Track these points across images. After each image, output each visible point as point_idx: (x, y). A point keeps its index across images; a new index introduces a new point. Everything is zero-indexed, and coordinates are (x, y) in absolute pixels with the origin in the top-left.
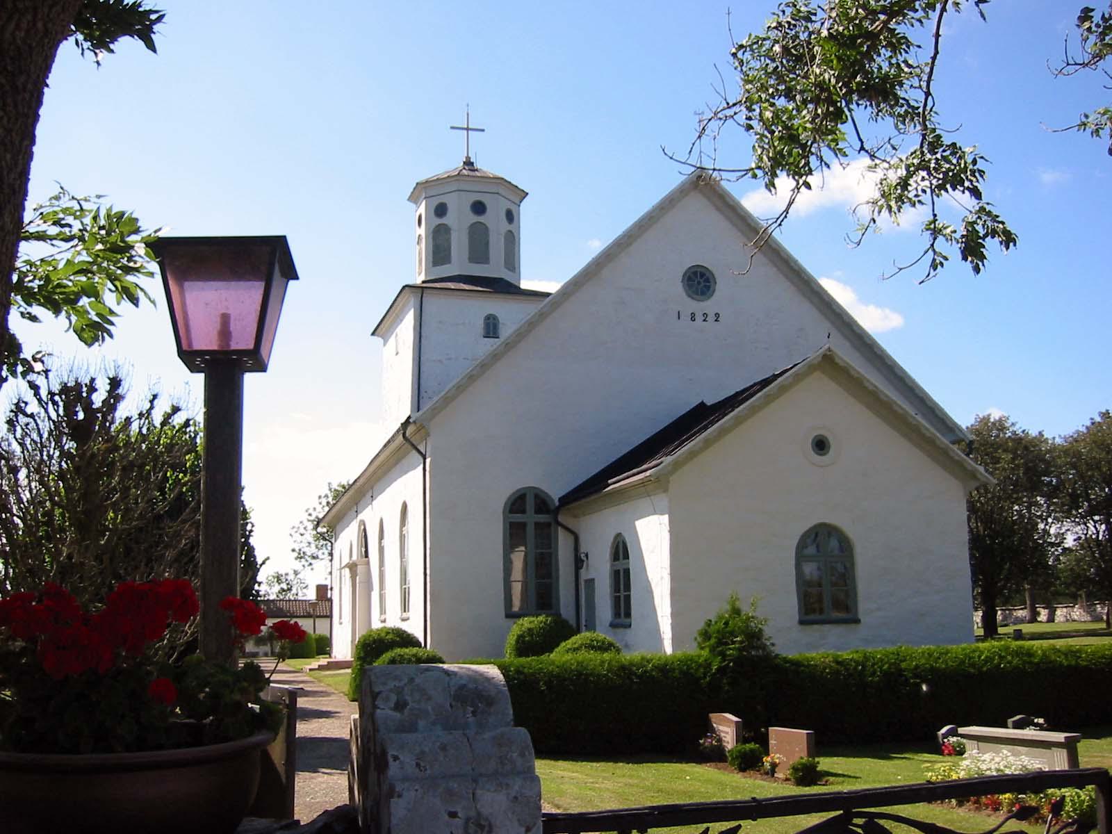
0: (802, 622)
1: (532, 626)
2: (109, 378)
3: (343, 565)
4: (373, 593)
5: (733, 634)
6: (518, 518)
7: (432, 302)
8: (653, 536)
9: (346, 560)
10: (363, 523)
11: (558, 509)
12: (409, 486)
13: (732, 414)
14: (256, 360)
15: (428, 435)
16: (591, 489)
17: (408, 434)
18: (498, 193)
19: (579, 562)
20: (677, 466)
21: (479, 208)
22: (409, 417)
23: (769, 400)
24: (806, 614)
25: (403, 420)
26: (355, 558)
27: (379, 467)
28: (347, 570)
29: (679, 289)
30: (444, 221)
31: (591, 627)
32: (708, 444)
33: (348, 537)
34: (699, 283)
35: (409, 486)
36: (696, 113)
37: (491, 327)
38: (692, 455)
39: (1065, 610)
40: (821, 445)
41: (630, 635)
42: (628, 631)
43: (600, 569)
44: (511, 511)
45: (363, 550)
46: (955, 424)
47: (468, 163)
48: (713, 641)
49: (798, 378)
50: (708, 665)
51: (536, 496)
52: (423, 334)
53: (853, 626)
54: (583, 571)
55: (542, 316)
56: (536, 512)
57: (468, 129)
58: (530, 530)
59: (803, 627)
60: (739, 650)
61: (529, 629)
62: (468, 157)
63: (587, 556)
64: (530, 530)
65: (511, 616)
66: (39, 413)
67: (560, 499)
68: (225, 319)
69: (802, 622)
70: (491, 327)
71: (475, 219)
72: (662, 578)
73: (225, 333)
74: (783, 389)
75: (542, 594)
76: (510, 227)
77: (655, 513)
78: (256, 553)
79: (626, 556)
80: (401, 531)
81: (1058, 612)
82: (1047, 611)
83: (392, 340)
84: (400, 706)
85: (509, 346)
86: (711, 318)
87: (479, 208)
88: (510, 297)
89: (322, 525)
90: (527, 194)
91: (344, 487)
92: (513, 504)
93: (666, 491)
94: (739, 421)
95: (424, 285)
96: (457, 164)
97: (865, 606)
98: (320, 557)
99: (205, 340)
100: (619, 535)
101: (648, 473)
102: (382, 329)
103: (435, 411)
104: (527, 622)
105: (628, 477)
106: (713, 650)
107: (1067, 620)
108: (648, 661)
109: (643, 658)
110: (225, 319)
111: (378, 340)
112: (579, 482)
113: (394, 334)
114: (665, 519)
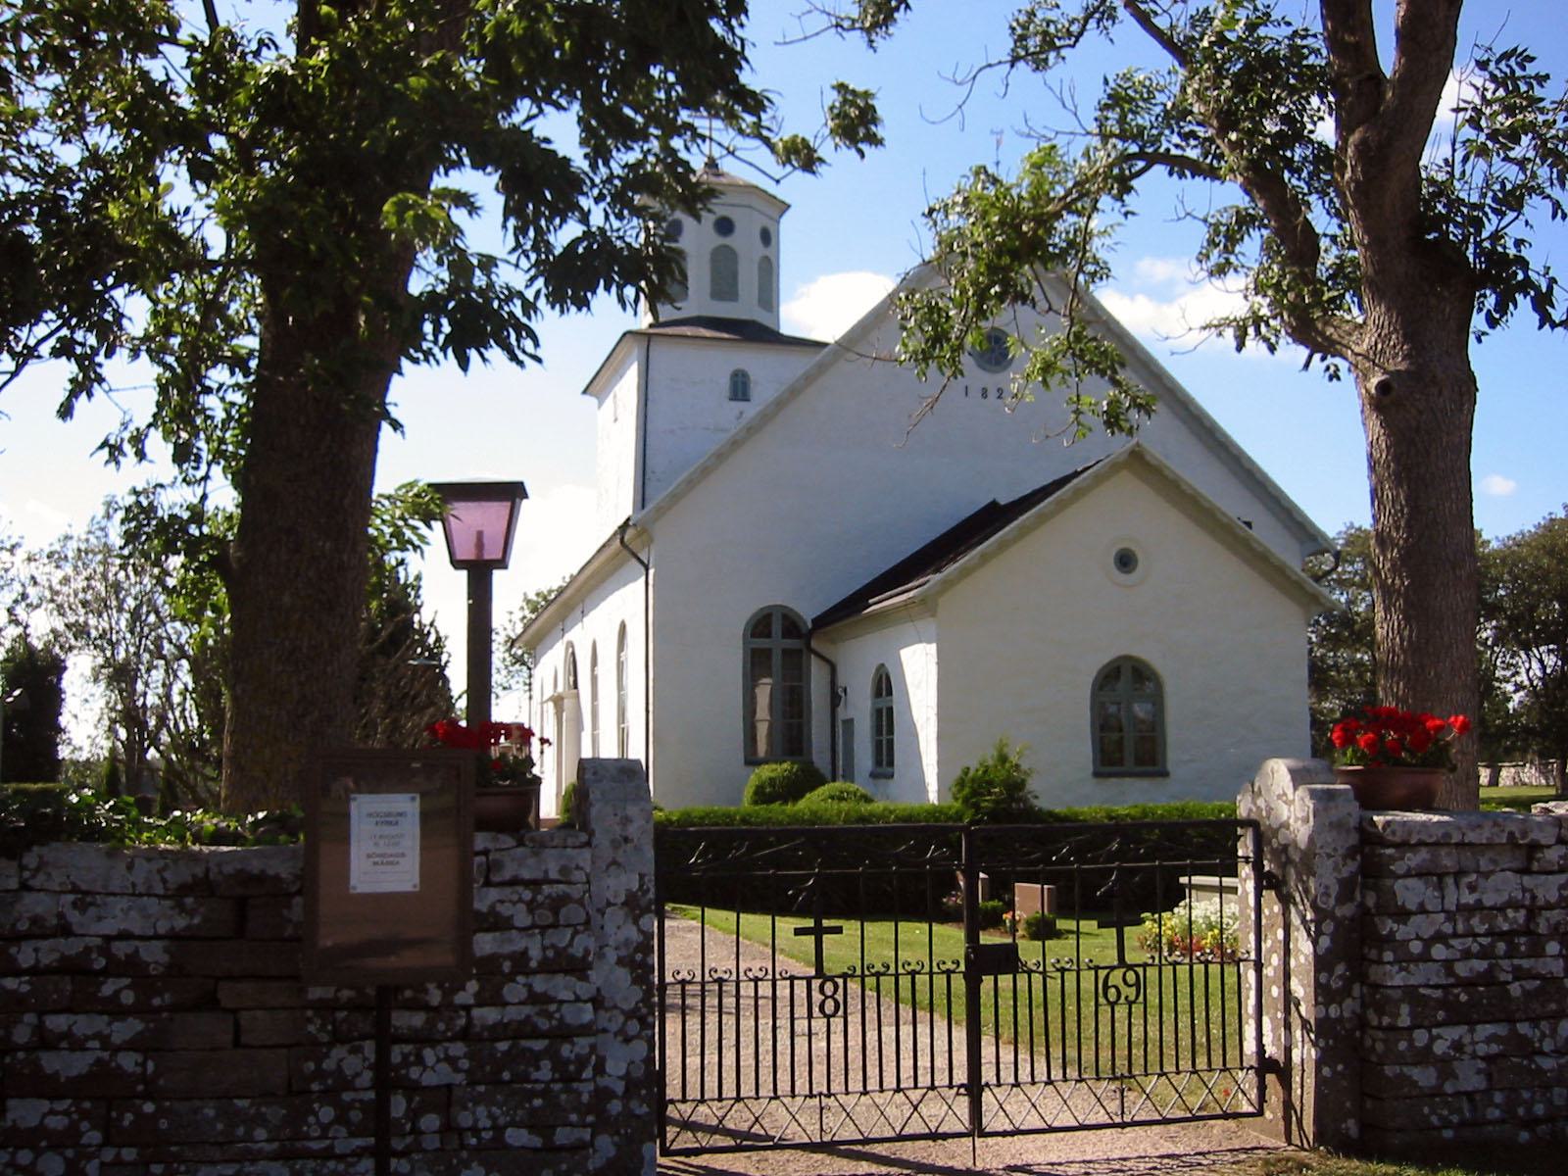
0: (1097, 774)
1: (773, 775)
3: (545, 698)
4: (583, 734)
5: (991, 783)
6: (762, 643)
7: (661, 352)
8: (919, 668)
9: (549, 692)
10: (570, 644)
11: (811, 633)
12: (627, 603)
13: (1015, 523)
14: (502, 563)
15: (651, 540)
16: (849, 610)
17: (626, 538)
18: (750, 207)
19: (836, 698)
20: (947, 585)
22: (628, 519)
23: (1062, 505)
24: (1103, 763)
25: (621, 522)
26: (560, 689)
27: (592, 576)
28: (551, 705)
31: (849, 776)
32: (985, 559)
33: (552, 660)
35: (627, 603)
36: (992, 132)
37: (740, 387)
38: (965, 573)
39: (1513, 770)
40: (1126, 561)
41: (894, 786)
42: (890, 781)
43: (860, 707)
44: (753, 635)
45: (572, 679)
46: (1318, 531)
48: (967, 791)
49: (1099, 480)
50: (959, 817)
52: (650, 397)
53: (1160, 779)
54: (840, 709)
55: (809, 379)
56: (784, 637)
58: (777, 659)
59: (1100, 780)
60: (997, 802)
61: (771, 779)
63: (845, 690)
64: (777, 659)
65: (752, 761)
67: (814, 621)
68: (480, 535)
69: (1097, 774)
70: (740, 387)
71: (721, 241)
72: (928, 719)
73: (480, 545)
74: (1079, 494)
75: (792, 738)
76: (767, 252)
77: (921, 642)
78: (451, 686)
79: (890, 693)
80: (619, 657)
81: (1504, 773)
82: (1488, 771)
83: (609, 401)
84: (595, 773)
85: (765, 418)
88: (769, 346)
89: (517, 645)
90: (789, 206)
91: (545, 599)
93: (933, 616)
94: (1023, 533)
95: (652, 331)
97: (1173, 756)
98: (514, 687)
99: (466, 553)
100: (883, 665)
101: (911, 594)
102: (597, 386)
103: (661, 511)
104: (766, 772)
105: (891, 597)
106: (966, 800)
107: (1515, 784)
108: (891, 812)
109: (885, 809)
110: (480, 535)
111: (592, 401)
112: (876, 574)
113: (612, 395)
114: (932, 648)
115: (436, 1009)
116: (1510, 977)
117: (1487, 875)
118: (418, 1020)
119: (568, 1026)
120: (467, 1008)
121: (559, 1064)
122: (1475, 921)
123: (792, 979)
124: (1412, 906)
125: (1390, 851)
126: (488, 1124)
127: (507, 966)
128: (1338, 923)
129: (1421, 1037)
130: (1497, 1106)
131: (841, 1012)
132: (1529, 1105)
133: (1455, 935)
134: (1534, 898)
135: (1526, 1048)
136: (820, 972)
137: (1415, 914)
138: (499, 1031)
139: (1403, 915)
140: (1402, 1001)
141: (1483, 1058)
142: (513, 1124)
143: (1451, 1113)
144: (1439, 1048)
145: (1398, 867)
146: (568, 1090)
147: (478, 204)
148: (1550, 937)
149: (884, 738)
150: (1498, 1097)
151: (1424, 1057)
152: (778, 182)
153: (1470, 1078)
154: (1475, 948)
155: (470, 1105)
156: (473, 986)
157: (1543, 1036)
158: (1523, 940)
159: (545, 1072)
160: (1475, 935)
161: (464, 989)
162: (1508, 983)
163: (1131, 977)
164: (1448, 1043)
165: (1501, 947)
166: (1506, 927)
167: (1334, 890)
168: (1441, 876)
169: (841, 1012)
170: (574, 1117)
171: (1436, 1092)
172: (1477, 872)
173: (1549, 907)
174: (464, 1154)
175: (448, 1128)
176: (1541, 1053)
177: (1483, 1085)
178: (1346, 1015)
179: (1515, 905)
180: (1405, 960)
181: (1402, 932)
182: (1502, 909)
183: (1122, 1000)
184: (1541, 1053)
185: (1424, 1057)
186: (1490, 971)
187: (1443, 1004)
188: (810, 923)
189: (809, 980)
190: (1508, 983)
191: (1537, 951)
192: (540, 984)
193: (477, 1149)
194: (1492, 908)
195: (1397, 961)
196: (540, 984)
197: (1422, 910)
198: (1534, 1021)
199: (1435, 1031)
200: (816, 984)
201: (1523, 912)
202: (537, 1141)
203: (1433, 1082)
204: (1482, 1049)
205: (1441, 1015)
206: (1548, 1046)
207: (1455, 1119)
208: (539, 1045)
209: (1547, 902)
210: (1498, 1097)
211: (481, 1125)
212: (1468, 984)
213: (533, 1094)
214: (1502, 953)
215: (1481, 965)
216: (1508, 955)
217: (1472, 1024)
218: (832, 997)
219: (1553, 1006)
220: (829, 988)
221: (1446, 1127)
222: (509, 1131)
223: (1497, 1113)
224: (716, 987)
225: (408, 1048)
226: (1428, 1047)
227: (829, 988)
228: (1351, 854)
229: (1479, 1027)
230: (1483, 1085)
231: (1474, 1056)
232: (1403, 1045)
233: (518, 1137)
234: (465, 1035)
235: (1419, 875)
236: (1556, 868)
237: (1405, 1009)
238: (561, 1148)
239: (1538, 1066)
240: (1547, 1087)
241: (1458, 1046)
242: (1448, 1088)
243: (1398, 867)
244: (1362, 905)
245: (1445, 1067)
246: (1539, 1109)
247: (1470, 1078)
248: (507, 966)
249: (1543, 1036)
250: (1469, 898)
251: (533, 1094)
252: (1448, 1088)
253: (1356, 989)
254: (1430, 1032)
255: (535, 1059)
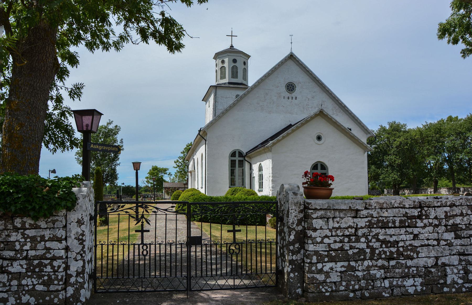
6: (233, 158)
21: (235, 61)
27: (197, 143)
40: (319, 138)
47: (232, 46)
51: (239, 152)
57: (232, 36)
62: (232, 45)
86: (294, 98)
87: (235, 61)
92: (232, 154)
96: (228, 47)
102: (205, 99)
115: (18, 250)
117: (342, 218)
118: (12, 254)
119: (55, 256)
120: (27, 250)
121: (53, 267)
122: (338, 232)
123: (134, 245)
125: (312, 211)
126: (32, 284)
127: (39, 239)
128: (297, 232)
129: (320, 266)
130: (343, 286)
131: (148, 255)
132: (354, 286)
133: (332, 236)
134: (357, 225)
135: (354, 269)
136: (142, 243)
138: (36, 257)
139: (315, 230)
142: (38, 284)
144: (325, 269)
145: (314, 216)
146: (55, 274)
147: (79, 45)
148: (362, 236)
150: (344, 283)
151: (320, 271)
153: (335, 278)
155: (26, 278)
156: (29, 244)
157: (359, 265)
159: (49, 269)
160: (338, 236)
161: (26, 245)
162: (348, 250)
163: (237, 247)
165: (346, 240)
166: (348, 234)
168: (328, 219)
169: (148, 255)
170: (56, 282)
171: (325, 281)
172: (340, 217)
173: (362, 228)
174: (24, 292)
175: (20, 285)
177: (339, 280)
180: (315, 243)
181: (314, 234)
182: (347, 228)
183: (234, 253)
185: (320, 271)
186: (342, 247)
187: (327, 256)
188: (232, 229)
189: (139, 245)
190: (348, 250)
191: (358, 241)
192: (48, 244)
193: (28, 291)
194: (344, 228)
195: (313, 243)
196: (48, 244)
198: (356, 261)
199: (324, 264)
200: (141, 246)
202: (46, 289)
203: (324, 279)
204: (339, 269)
205: (326, 259)
207: (329, 290)
208: (47, 262)
210: (344, 283)
211: (28, 284)
212: (335, 250)
213: (45, 275)
216: (349, 242)
218: (146, 250)
219: (362, 257)
220: (145, 248)
222: (37, 286)
223: (343, 288)
225: (7, 262)
226: (322, 269)
227: (145, 248)
228: (301, 212)
229: (338, 263)
230: (339, 280)
231: (336, 271)
232: (314, 268)
233: (40, 288)
234: (26, 258)
235: (321, 218)
238: (52, 291)
241: (332, 269)
242: (328, 280)
243: (314, 216)
244: (304, 227)
245: (327, 274)
246: (357, 287)
247: (335, 278)
248: (39, 239)
249: (359, 265)
250: (337, 225)
251: (45, 275)
253: (302, 252)
255: (45, 266)
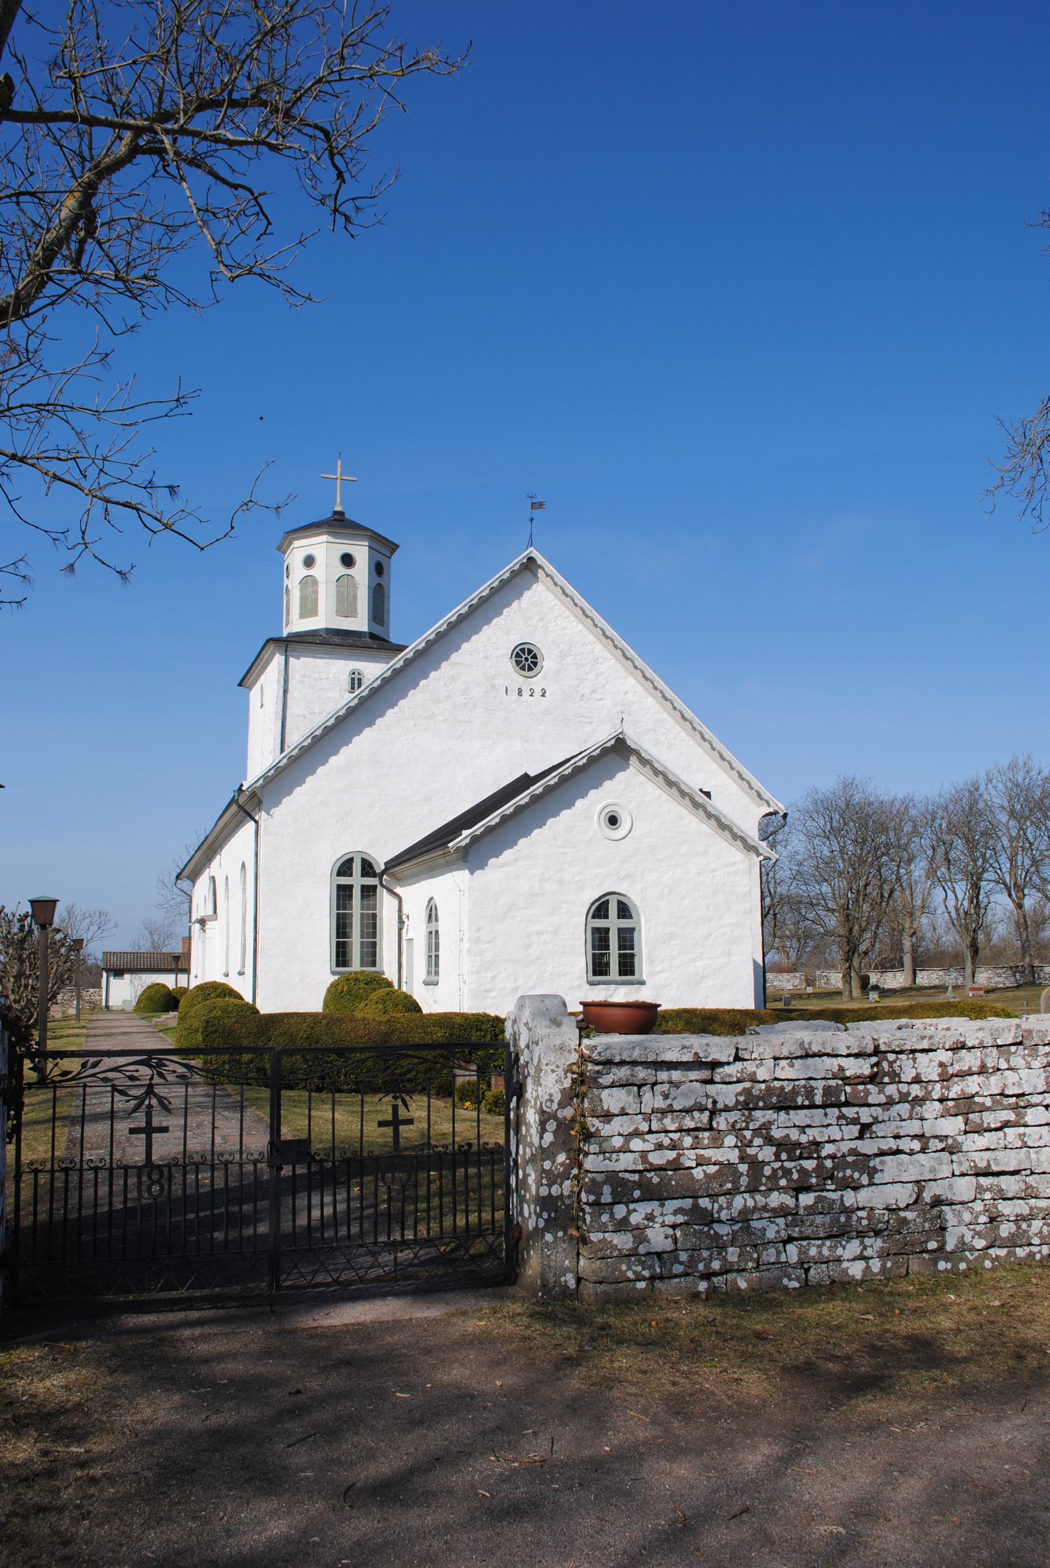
2: (505, 1020)
29: (508, 665)
30: (312, 572)
34: (527, 660)
44: (339, 874)
56: (363, 876)
58: (357, 893)
66: (941, 1065)
71: (344, 571)
116: (694, 1164)
124: (615, 1110)
130: (681, 1263)
133: (650, 1132)
135: (708, 1219)
137: (617, 1115)
139: (607, 1117)
140: (605, 1182)
141: (670, 1226)
143: (644, 1269)
149: (433, 954)
151: (622, 1226)
152: (202, 549)
154: (666, 1142)
158: (706, 1134)
160: (667, 1132)
164: (643, 1216)
167: (557, 1097)
171: (633, 1253)
173: (727, 1109)
176: (720, 1221)
178: (566, 1193)
179: (702, 1109)
181: (606, 1130)
182: (688, 1111)
184: (720, 1221)
187: (639, 1185)
190: (692, 1168)
197: (623, 1113)
198: (713, 1197)
199: (632, 1206)
201: (707, 1113)
204: (670, 1219)
205: (637, 1194)
206: (724, 1215)
207: (646, 1273)
209: (726, 1106)
214: (688, 1146)
215: (672, 1155)
217: (662, 1200)
219: (729, 1186)
221: (640, 1280)
224: (32, 1176)
236: (735, 1079)
237: (607, 1190)
239: (716, 1233)
240: (723, 1248)
241: (650, 1217)
249: (721, 1208)
252: (642, 1250)
254: (628, 1207)
